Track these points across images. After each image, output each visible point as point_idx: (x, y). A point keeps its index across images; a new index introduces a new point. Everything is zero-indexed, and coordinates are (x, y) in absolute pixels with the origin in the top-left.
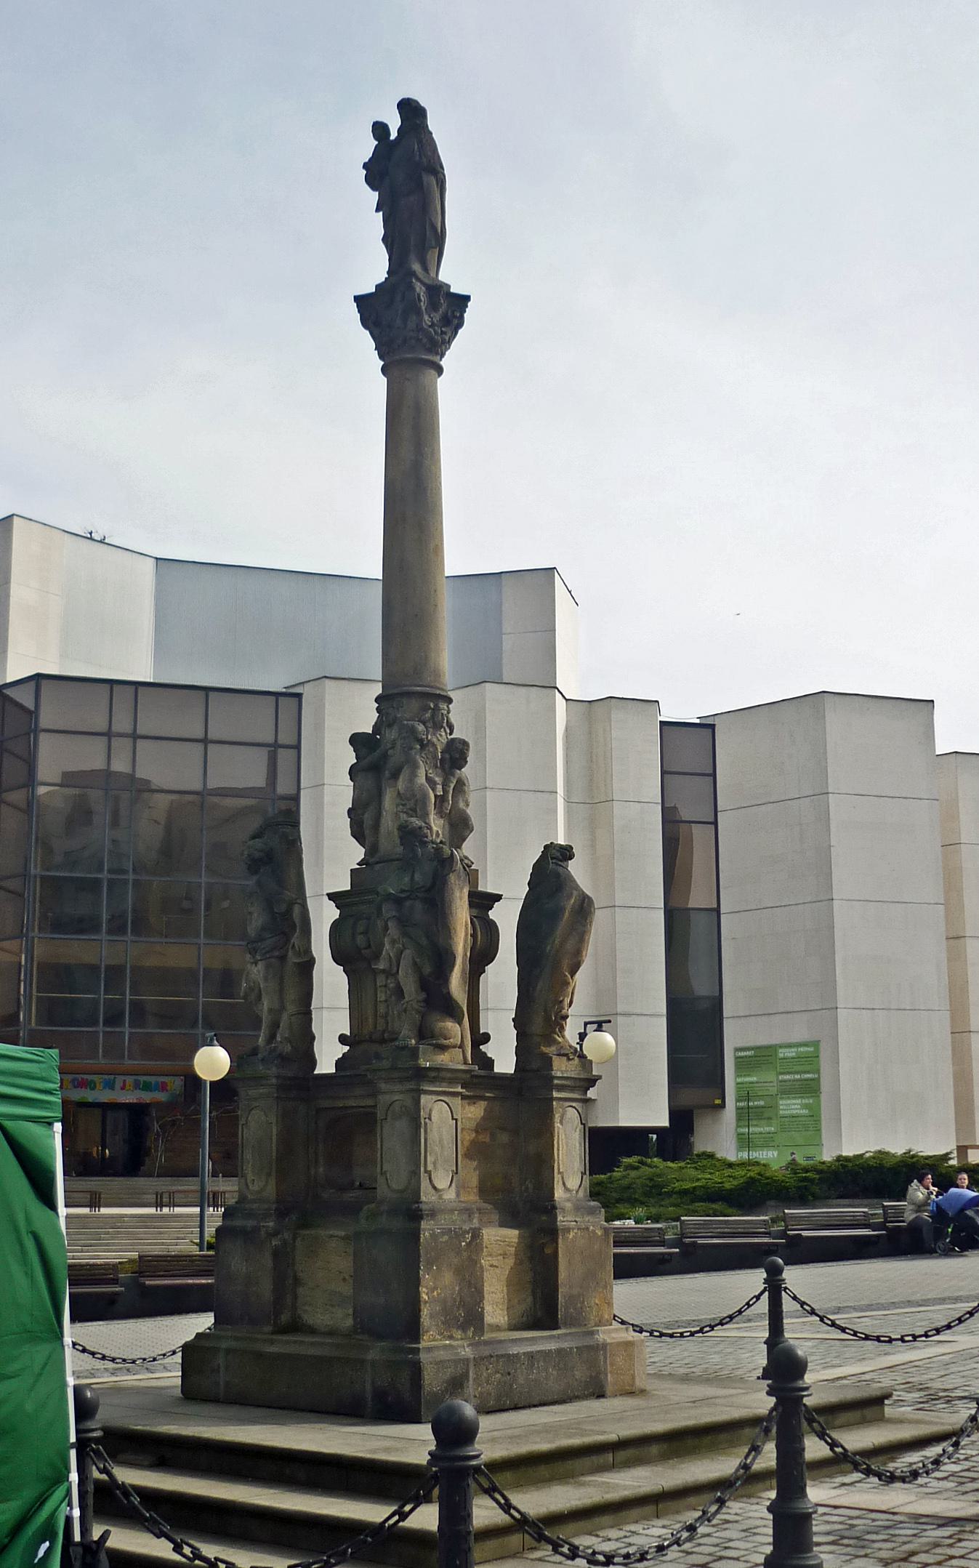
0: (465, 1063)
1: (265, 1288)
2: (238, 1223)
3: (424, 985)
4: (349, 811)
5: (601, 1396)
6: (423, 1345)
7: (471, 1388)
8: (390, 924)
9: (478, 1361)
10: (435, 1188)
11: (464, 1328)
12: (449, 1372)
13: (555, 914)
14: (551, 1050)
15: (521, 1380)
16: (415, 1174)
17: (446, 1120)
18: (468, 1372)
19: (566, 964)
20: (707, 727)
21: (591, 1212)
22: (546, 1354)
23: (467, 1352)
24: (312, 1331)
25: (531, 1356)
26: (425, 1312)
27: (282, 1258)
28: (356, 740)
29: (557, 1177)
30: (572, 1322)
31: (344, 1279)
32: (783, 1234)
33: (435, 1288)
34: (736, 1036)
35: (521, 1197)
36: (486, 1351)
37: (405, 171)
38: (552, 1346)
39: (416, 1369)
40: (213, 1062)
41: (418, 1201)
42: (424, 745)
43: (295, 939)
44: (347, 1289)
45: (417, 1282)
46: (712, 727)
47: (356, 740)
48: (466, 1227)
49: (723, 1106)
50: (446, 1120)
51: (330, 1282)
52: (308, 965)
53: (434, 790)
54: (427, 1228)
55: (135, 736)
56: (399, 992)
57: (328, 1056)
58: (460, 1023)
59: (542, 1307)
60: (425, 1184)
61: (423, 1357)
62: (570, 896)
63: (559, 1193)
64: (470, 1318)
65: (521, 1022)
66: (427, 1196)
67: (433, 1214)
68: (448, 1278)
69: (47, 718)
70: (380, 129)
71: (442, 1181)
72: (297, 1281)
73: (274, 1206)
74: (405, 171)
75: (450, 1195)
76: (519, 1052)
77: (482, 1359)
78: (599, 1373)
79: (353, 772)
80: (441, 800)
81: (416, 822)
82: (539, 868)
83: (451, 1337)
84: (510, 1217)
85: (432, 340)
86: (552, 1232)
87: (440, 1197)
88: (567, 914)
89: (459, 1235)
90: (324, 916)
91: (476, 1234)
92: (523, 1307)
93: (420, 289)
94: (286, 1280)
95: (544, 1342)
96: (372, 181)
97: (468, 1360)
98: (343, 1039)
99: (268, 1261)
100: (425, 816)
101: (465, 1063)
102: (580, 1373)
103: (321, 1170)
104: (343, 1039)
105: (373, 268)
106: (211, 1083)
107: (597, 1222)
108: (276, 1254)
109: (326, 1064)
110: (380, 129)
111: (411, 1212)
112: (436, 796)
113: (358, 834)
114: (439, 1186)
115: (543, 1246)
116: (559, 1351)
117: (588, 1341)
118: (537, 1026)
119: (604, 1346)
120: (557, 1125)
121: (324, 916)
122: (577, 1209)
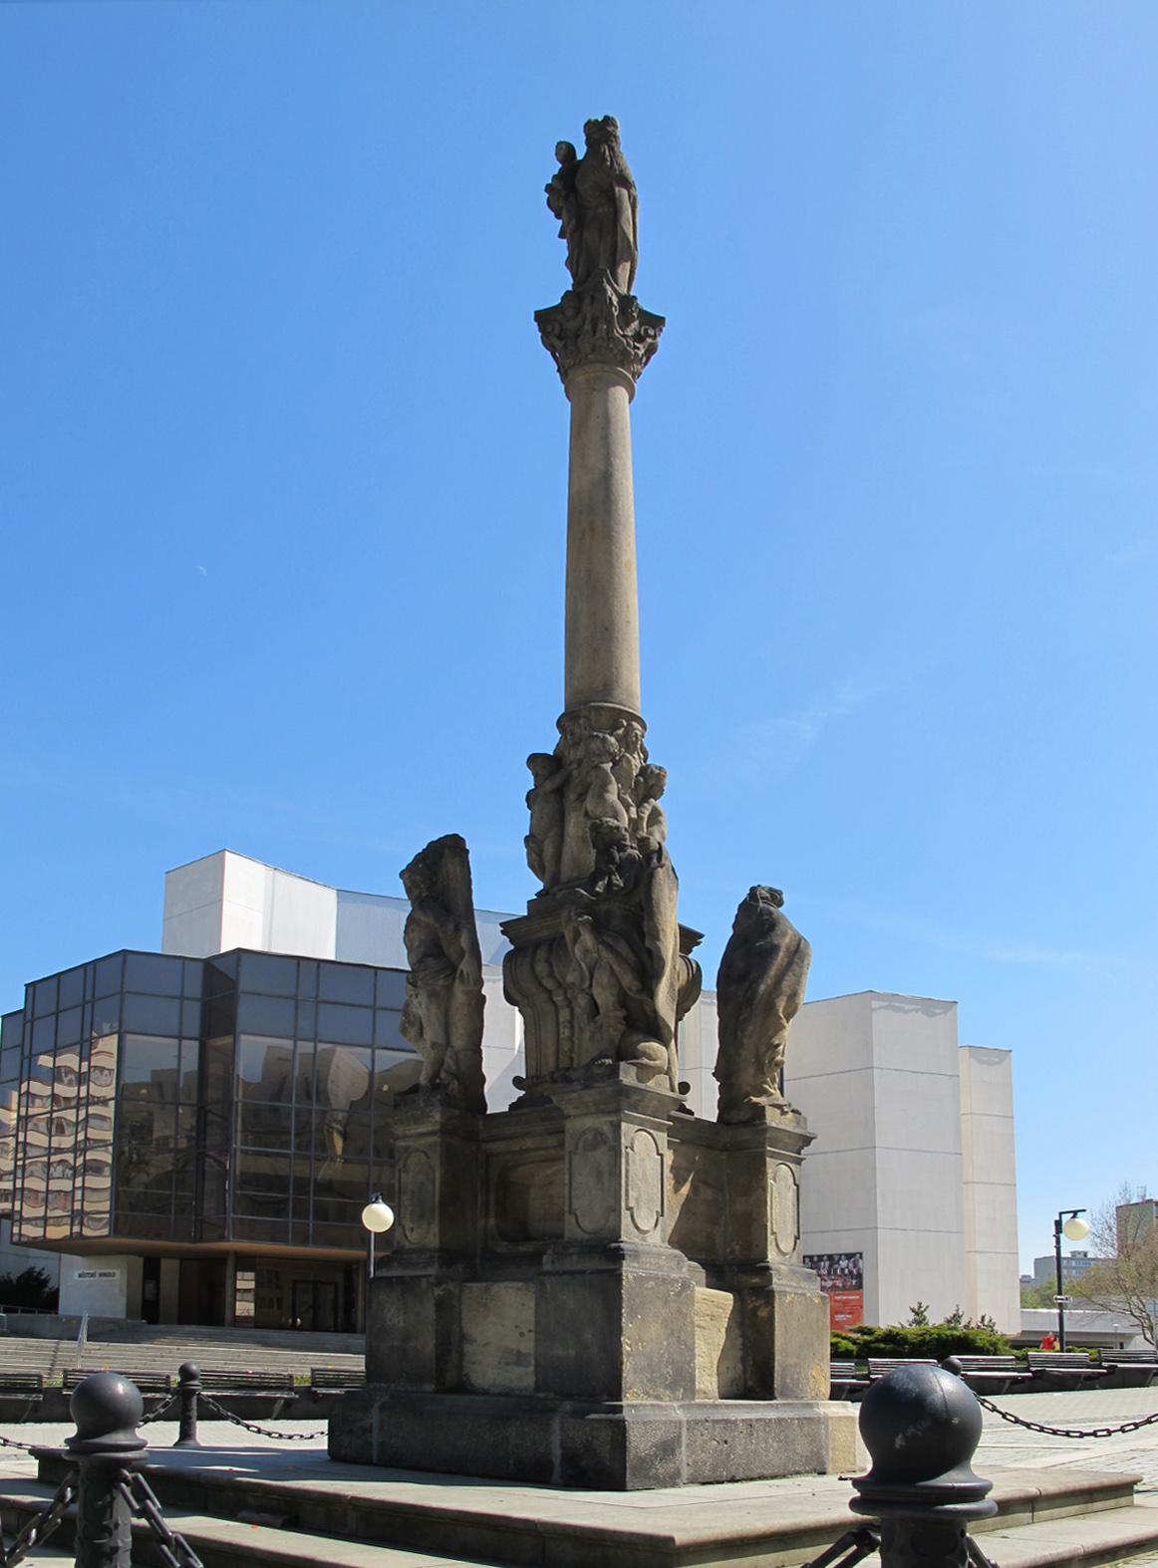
0: (673, 1090)
1: (427, 1345)
3: (623, 999)
4: (527, 839)
5: (822, 1473)
6: (624, 1403)
7: (683, 1456)
8: (581, 929)
9: (693, 1425)
10: (637, 1228)
11: (672, 1386)
12: (660, 1435)
14: (762, 1100)
15: (739, 1450)
16: (616, 1210)
17: (646, 1159)
18: (680, 1437)
22: (767, 1422)
23: (680, 1415)
25: (750, 1423)
27: (447, 1309)
28: (534, 760)
29: (770, 1238)
31: (522, 1334)
36: (700, 1415)
37: (589, 193)
38: (772, 1415)
39: (620, 1428)
41: (617, 1237)
43: (465, 966)
45: (619, 1331)
47: (534, 760)
48: (674, 1275)
50: (646, 1159)
53: (627, 811)
54: (629, 1270)
55: (318, 1002)
56: (594, 1009)
58: (667, 1046)
61: (626, 1414)
62: (784, 935)
63: (772, 1256)
64: (682, 1381)
66: (628, 1238)
67: (636, 1255)
68: (654, 1330)
69: (244, 984)
70: (566, 152)
72: (463, 1338)
73: (437, 1255)
74: (589, 193)
76: (722, 1104)
77: (696, 1422)
78: (821, 1447)
83: (658, 1397)
84: (718, 1278)
85: (625, 353)
86: (767, 1295)
87: (644, 1240)
88: (781, 954)
90: (493, 945)
92: (731, 1375)
97: (680, 1422)
98: (518, 1082)
99: (429, 1312)
101: (673, 1090)
102: (802, 1447)
103: (492, 1221)
104: (518, 1082)
105: (555, 283)
106: (375, 1233)
108: (440, 1305)
110: (566, 152)
111: (607, 1252)
112: (630, 819)
114: (643, 1227)
115: (755, 1310)
116: (780, 1421)
117: (807, 1413)
118: (747, 1076)
120: (770, 1181)
121: (493, 945)
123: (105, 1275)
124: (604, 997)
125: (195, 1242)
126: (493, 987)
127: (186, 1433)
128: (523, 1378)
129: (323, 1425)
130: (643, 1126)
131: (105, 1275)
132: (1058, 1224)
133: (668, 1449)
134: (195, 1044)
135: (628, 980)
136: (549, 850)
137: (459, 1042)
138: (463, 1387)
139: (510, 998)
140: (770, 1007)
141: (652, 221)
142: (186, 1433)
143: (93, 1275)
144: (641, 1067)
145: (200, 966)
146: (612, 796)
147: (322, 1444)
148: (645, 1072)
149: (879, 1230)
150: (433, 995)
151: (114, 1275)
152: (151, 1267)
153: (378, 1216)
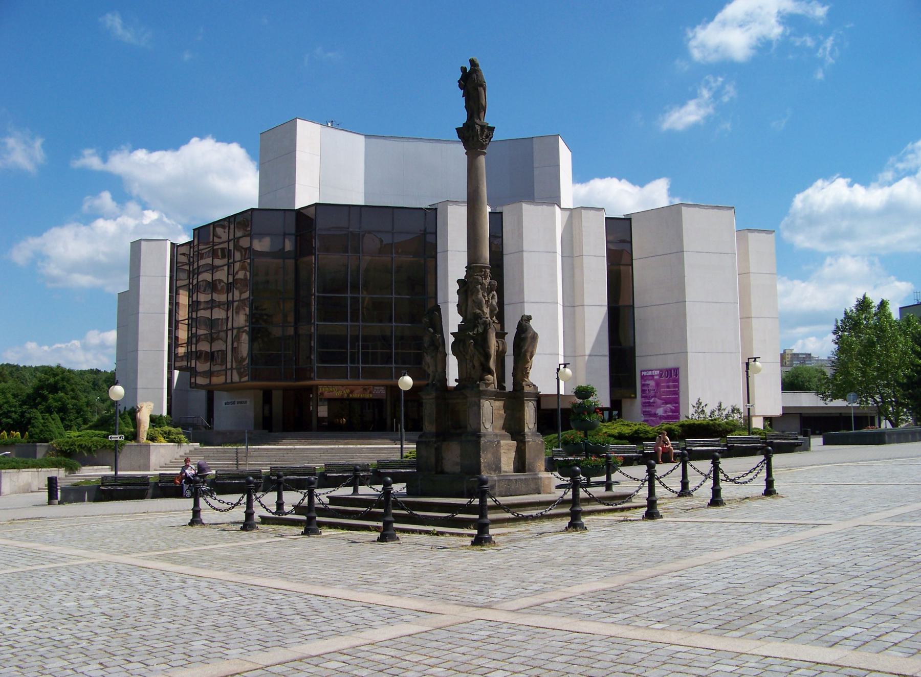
1: (433, 460)
2: (423, 439)
9: (499, 481)
11: (495, 471)
13: (524, 339)
19: (528, 355)
20: (627, 221)
21: (538, 436)
22: (521, 480)
23: (496, 478)
24: (447, 473)
25: (516, 480)
26: (482, 465)
27: (438, 451)
28: (459, 281)
30: (530, 470)
32: (642, 452)
33: (485, 458)
34: (642, 364)
35: (514, 429)
37: (471, 83)
38: (523, 477)
40: (407, 382)
41: (480, 431)
42: (482, 284)
43: (440, 349)
44: (458, 460)
46: (630, 219)
47: (459, 281)
49: (636, 397)
51: (453, 456)
52: (445, 355)
54: (483, 441)
56: (474, 367)
57: (452, 383)
59: (521, 465)
60: (482, 427)
63: (526, 430)
64: (498, 468)
65: (514, 375)
66: (483, 430)
67: (485, 435)
68: (489, 455)
70: (464, 69)
71: (488, 425)
74: (471, 83)
75: (490, 430)
79: (458, 292)
80: (487, 302)
81: (478, 311)
82: (520, 324)
89: (493, 442)
91: (499, 442)
93: (478, 128)
94: (439, 459)
95: (521, 476)
96: (461, 87)
100: (481, 308)
102: (532, 486)
107: (540, 439)
108: (436, 449)
109: (452, 383)
110: (464, 69)
113: (460, 312)
119: (541, 478)
122: (533, 434)
123: (241, 403)
124: (477, 364)
125: (297, 380)
126: (449, 350)
127: (355, 491)
128: (457, 469)
129: (404, 485)
130: (487, 399)
131: (241, 403)
132: (747, 364)
133: (493, 487)
134: (293, 261)
135: (482, 359)
136: (463, 309)
137: (439, 370)
138: (442, 472)
139: (454, 354)
140: (525, 355)
141: (492, 98)
142: (355, 491)
143: (233, 403)
144: (486, 384)
145: (294, 213)
146: (480, 296)
147: (405, 490)
148: (488, 385)
149: (754, 321)
150: (432, 357)
151: (246, 402)
152: (267, 396)
153: (406, 383)
